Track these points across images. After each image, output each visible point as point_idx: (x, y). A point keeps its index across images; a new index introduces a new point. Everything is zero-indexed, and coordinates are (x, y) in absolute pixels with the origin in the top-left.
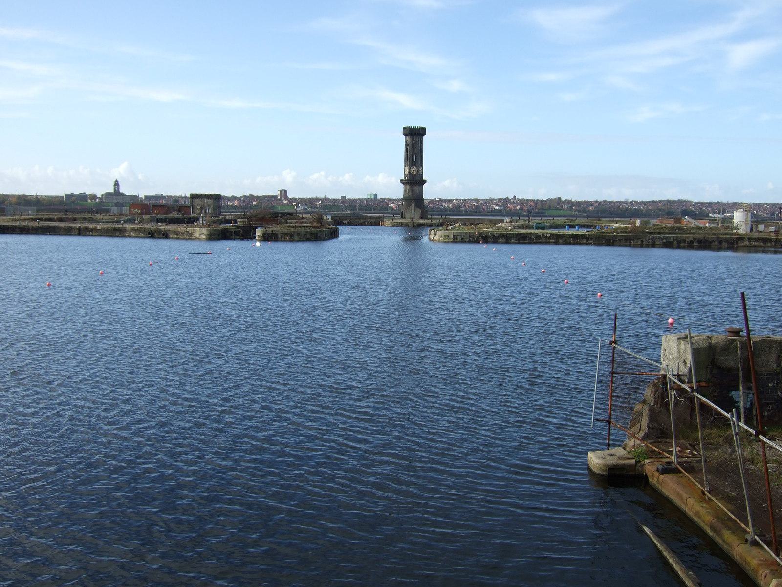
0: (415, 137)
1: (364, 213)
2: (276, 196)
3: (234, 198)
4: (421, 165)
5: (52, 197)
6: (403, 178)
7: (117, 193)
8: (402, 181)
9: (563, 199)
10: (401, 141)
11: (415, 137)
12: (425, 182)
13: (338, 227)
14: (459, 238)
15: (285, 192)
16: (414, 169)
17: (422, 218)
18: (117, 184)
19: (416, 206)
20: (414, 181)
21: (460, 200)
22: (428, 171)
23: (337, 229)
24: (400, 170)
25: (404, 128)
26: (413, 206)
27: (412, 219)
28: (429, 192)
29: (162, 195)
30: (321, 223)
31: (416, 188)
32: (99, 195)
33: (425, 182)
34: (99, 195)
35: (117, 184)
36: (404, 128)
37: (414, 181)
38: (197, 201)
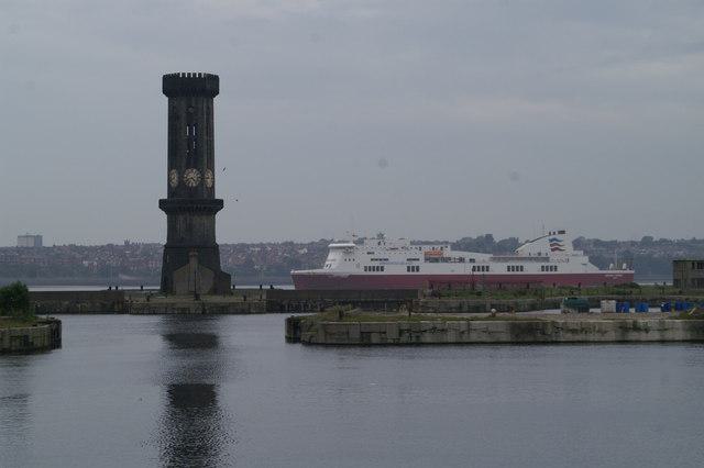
0: (190, 98)
4: (211, 165)
6: (165, 196)
8: (163, 204)
11: (190, 98)
12: (219, 204)
13: (56, 317)
14: (375, 339)
16: (192, 176)
17: (214, 291)
19: (200, 262)
20: (190, 203)
21: (253, 245)
23: (59, 323)
26: (194, 263)
27: (197, 297)
28: (228, 229)
31: (197, 220)
33: (219, 204)
37: (190, 203)
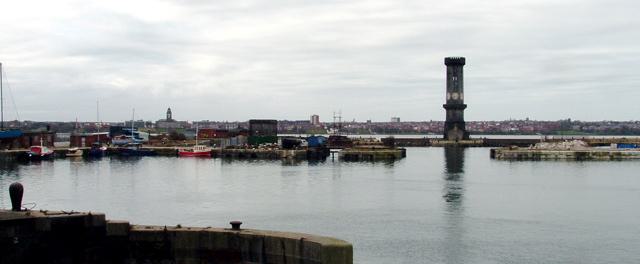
0: (455, 65)
1: (386, 146)
2: (308, 122)
3: (214, 123)
5: (380, 123)
7: (169, 120)
9: (572, 120)
10: (442, 73)
11: (455, 65)
12: (466, 106)
15: (318, 117)
16: (455, 96)
17: (464, 139)
18: (169, 112)
20: (455, 107)
22: (469, 96)
24: (442, 97)
25: (446, 59)
28: (469, 116)
29: (369, 122)
30: (454, 123)
31: (458, 112)
32: (154, 122)
33: (466, 106)
34: (154, 122)
35: (169, 112)
36: (446, 59)
37: (455, 107)
38: (256, 126)
